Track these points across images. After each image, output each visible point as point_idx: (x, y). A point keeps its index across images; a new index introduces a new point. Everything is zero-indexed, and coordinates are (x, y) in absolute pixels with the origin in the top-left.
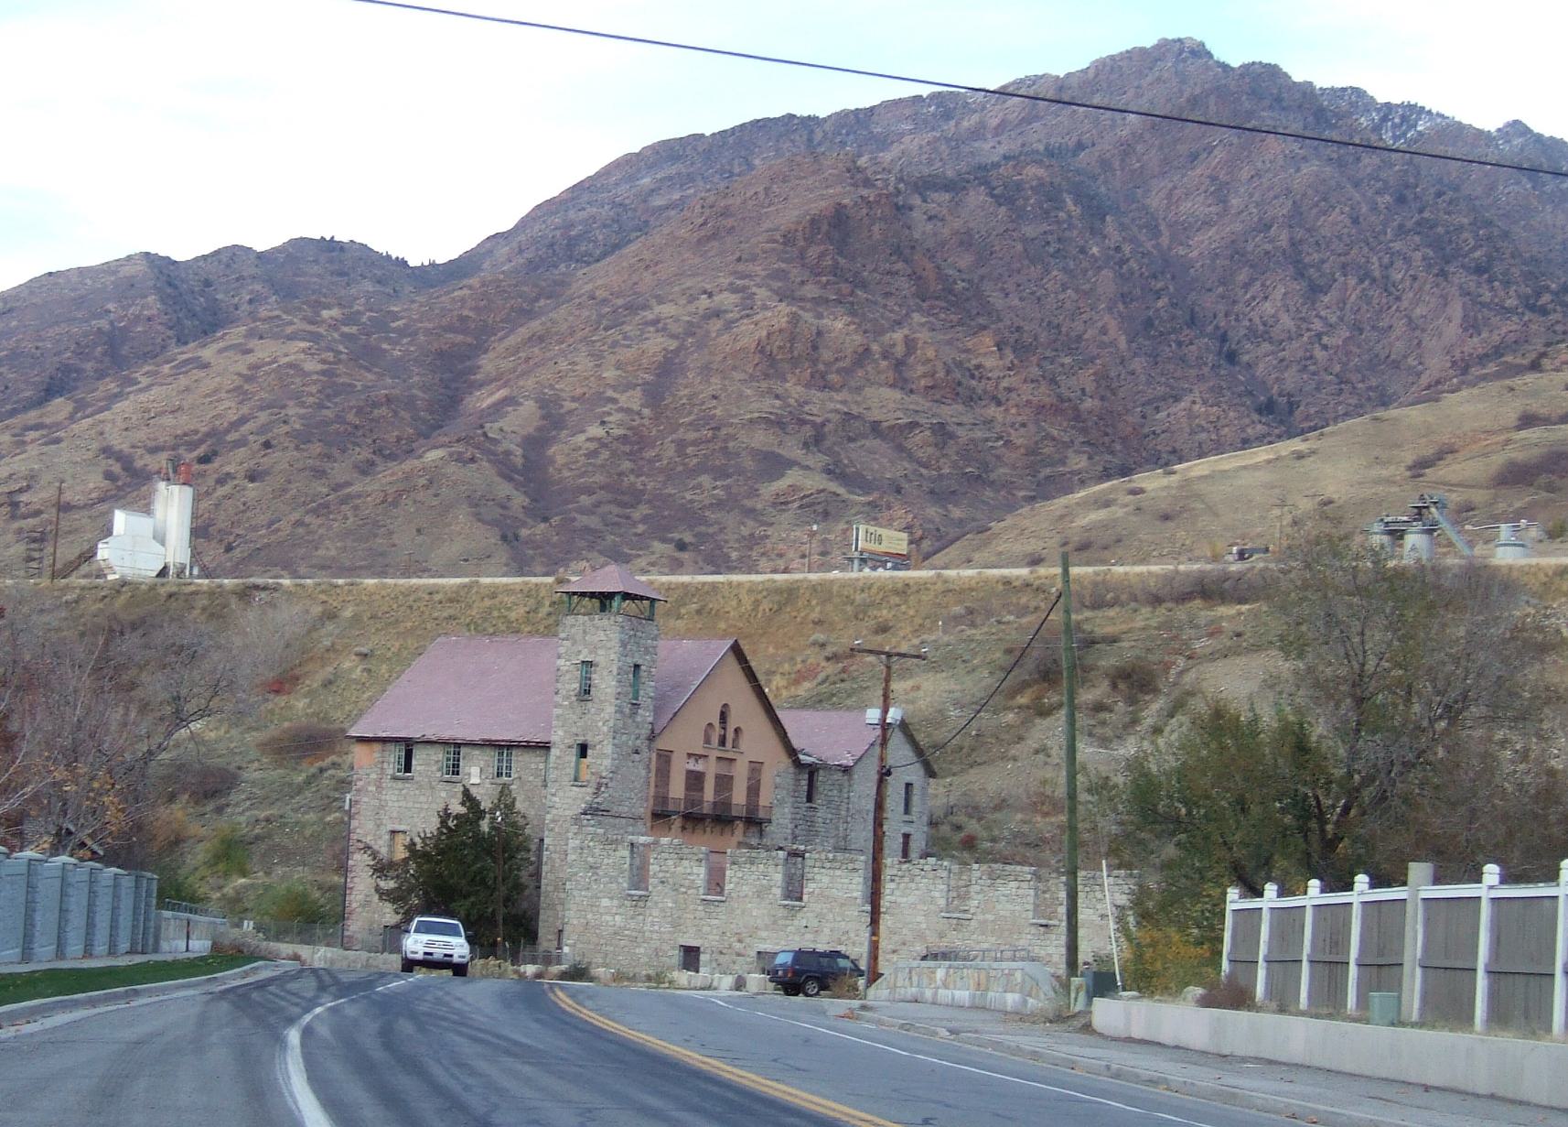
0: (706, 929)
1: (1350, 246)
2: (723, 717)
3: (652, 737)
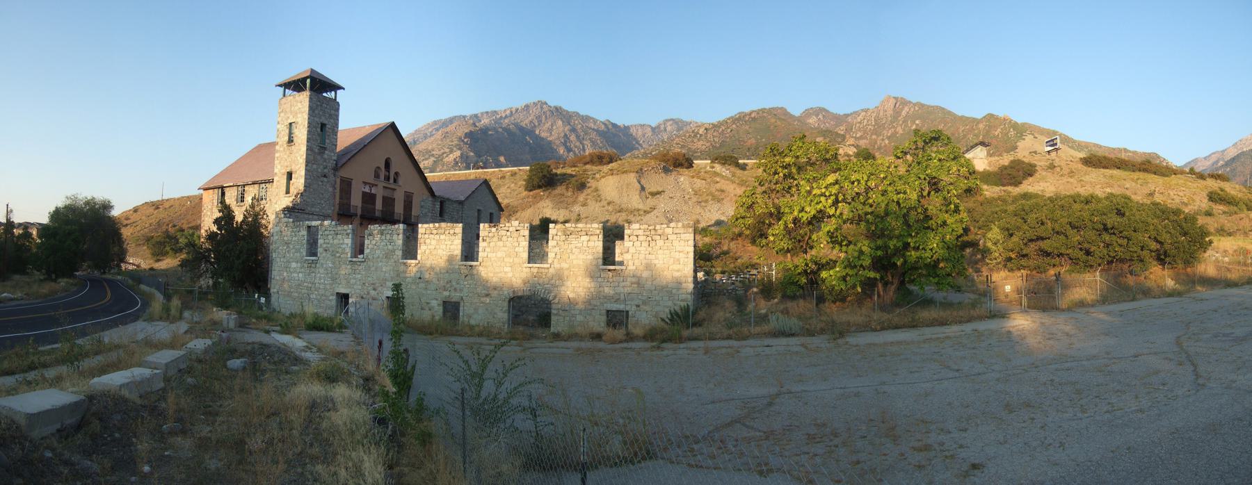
0: (353, 281)
2: (388, 164)
3: (336, 169)
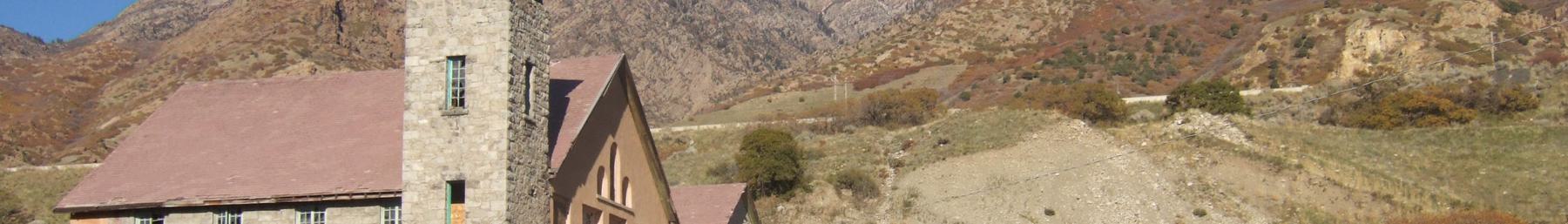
1: (646, 31)
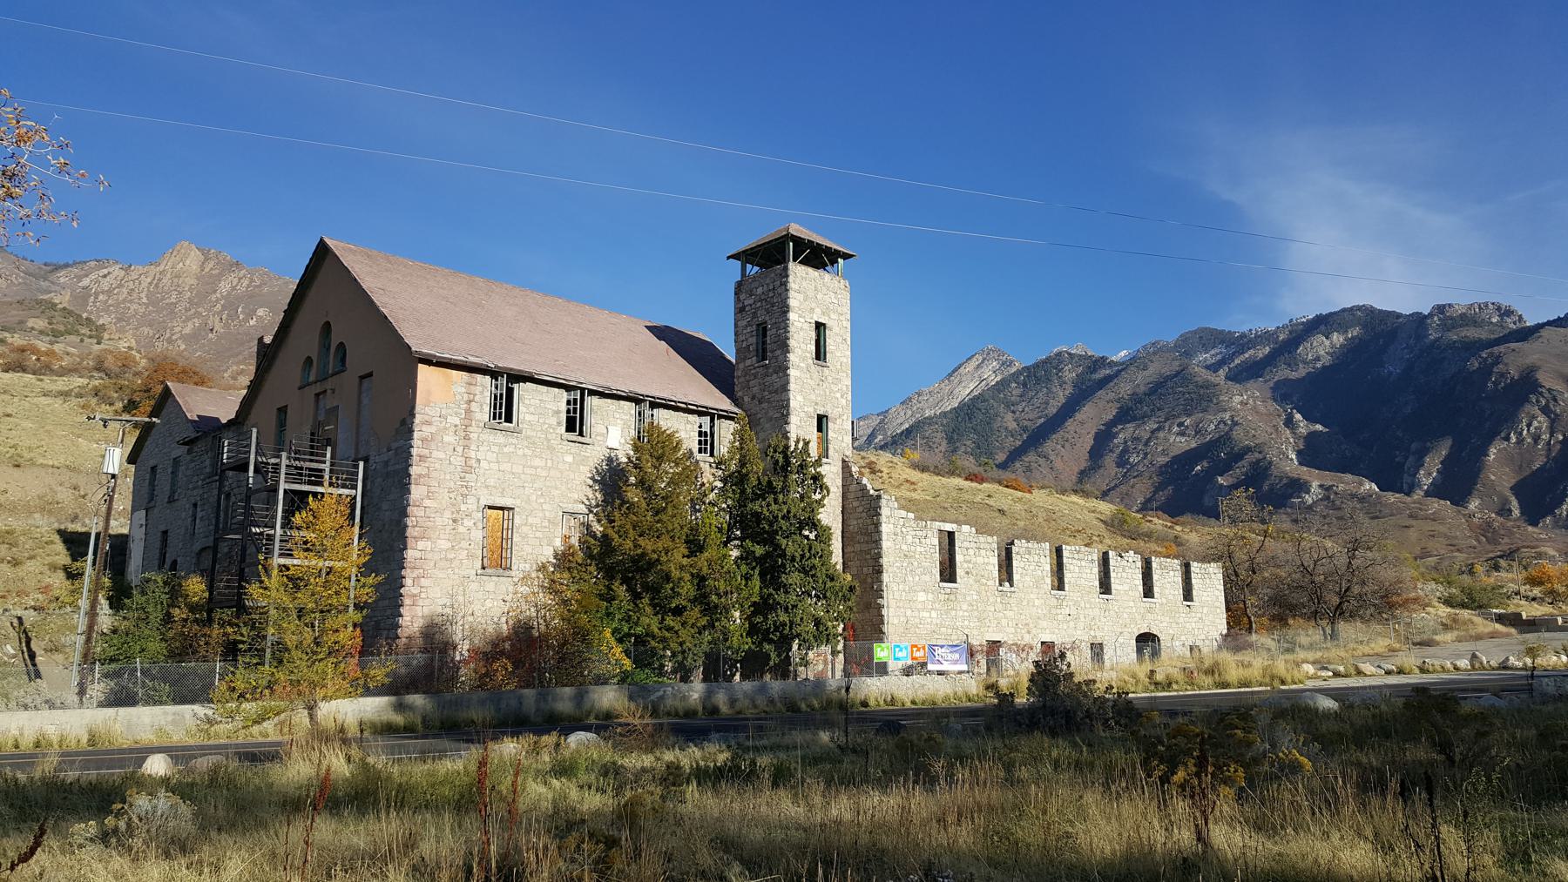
0: (1004, 622)
